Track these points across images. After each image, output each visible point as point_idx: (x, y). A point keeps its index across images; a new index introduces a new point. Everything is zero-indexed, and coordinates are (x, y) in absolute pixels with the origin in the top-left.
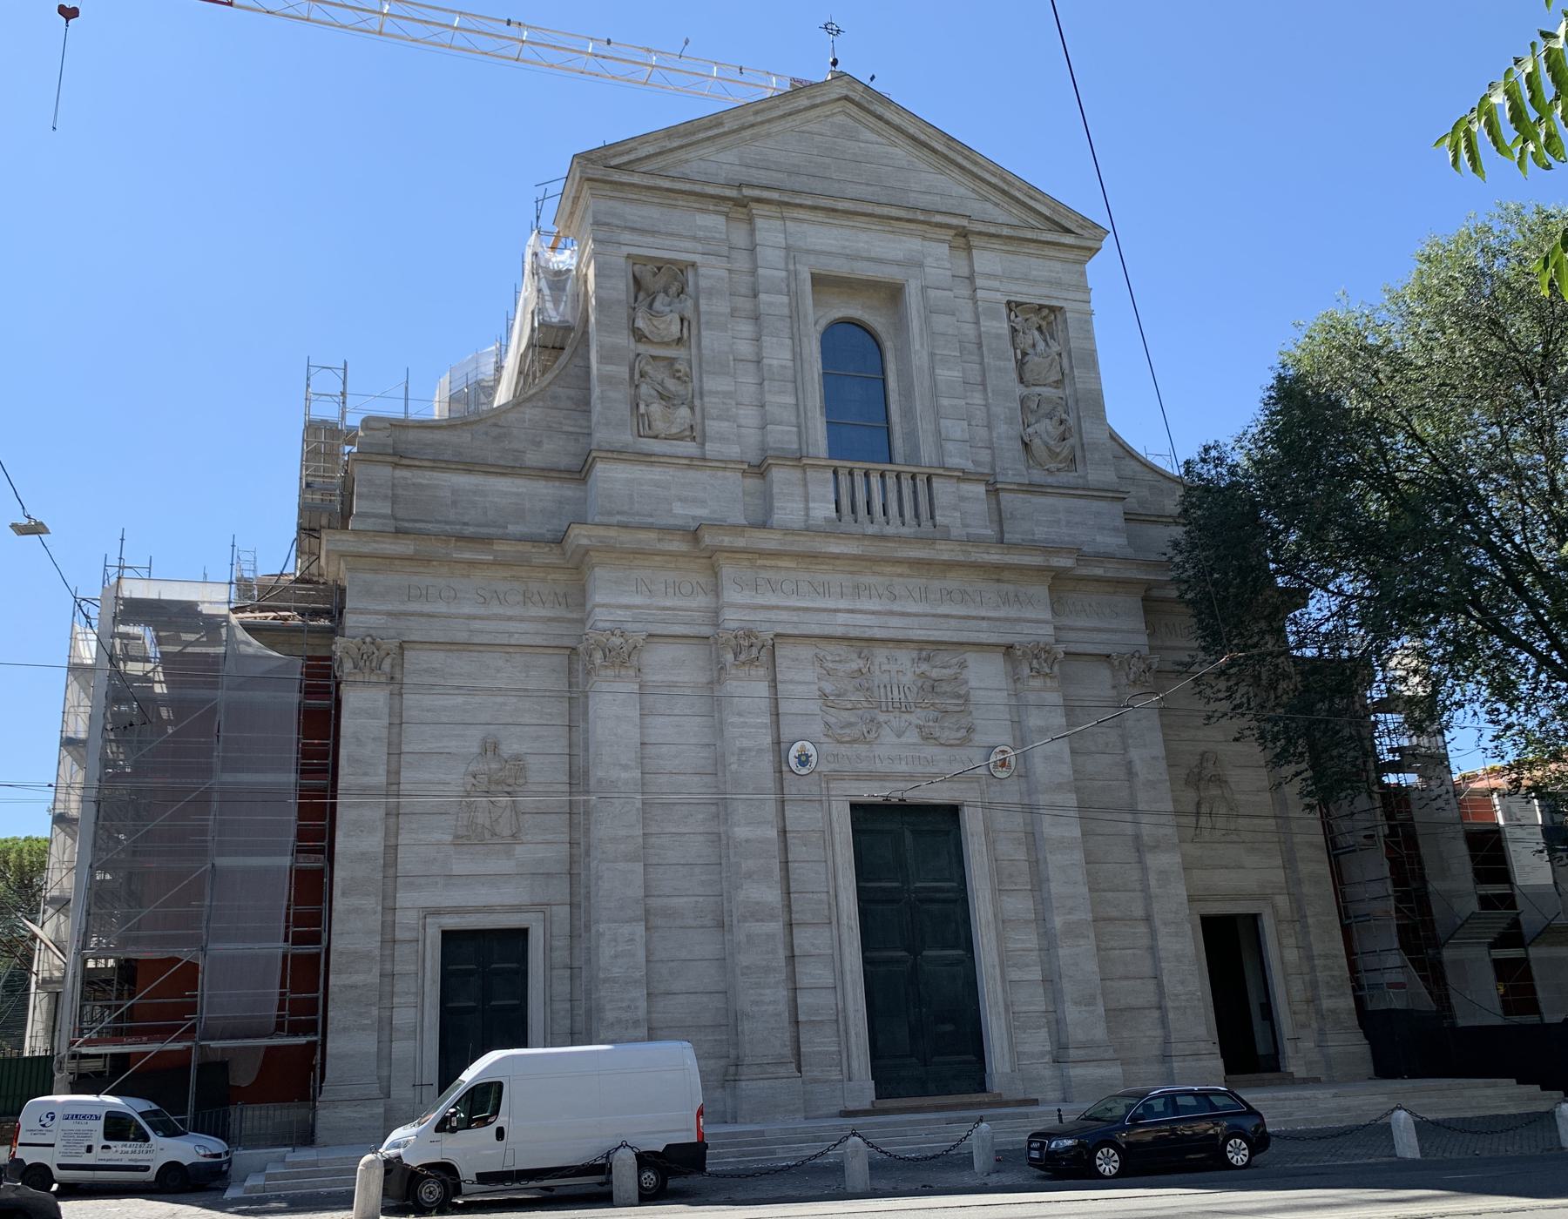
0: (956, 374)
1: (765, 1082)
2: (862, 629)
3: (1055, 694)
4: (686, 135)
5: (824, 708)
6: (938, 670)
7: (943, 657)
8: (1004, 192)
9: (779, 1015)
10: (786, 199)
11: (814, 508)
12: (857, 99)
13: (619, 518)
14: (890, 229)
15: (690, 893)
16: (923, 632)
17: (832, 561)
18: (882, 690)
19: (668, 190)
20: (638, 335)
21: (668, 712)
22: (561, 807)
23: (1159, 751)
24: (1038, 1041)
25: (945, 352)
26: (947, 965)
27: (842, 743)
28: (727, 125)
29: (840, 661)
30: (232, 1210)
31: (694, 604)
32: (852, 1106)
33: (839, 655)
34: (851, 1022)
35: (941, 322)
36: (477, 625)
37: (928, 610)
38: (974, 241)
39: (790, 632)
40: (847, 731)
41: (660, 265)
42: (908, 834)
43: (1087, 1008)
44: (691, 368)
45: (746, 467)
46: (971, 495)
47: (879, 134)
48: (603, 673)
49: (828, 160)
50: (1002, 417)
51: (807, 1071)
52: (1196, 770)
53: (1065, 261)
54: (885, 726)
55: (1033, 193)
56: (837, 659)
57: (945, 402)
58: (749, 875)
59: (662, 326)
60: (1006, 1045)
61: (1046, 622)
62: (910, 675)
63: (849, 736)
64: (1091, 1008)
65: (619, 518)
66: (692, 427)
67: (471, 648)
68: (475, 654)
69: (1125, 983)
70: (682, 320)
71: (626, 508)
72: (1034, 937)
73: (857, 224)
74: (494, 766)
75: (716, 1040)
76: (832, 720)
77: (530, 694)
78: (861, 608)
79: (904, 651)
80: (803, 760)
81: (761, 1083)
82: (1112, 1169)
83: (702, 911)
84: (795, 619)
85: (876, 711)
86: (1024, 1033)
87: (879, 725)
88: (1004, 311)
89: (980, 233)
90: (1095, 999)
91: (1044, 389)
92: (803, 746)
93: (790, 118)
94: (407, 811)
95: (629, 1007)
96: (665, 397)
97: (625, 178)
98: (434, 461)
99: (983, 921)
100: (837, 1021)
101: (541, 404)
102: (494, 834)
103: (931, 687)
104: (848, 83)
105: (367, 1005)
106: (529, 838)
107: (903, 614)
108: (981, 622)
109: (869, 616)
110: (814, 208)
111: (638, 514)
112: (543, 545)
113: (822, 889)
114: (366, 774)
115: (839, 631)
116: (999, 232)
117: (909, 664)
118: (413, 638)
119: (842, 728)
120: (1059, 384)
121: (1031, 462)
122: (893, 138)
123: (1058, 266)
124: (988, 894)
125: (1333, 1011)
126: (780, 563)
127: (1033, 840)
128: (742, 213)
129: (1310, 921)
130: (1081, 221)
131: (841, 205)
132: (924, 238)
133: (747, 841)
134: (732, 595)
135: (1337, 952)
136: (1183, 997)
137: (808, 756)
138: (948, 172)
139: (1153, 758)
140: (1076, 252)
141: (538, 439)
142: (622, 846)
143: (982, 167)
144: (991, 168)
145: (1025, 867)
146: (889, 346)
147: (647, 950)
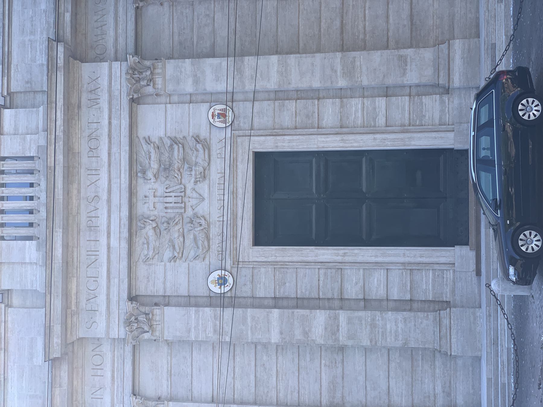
1: (452, 337)
2: (122, 226)
5: (183, 259)
6: (152, 162)
9: (405, 320)
11: (30, 259)
15: (318, 369)
16: (123, 175)
17: (70, 249)
18: (169, 211)
21: (189, 378)
27: (209, 246)
29: (148, 243)
30: (512, 191)
31: (109, 355)
32: (473, 267)
33: (144, 244)
34: (412, 260)
37: (105, 169)
39: (126, 286)
40: (200, 243)
43: (409, 64)
51: (446, 297)
54: (196, 210)
56: (146, 246)
58: (306, 333)
60: (434, 135)
62: (156, 186)
64: (409, 60)
69: (391, 20)
72: (354, 101)
75: (422, 359)
76: (192, 254)
79: (138, 189)
80: (222, 281)
81: (454, 340)
83: (332, 362)
84: (116, 280)
86: (425, 116)
87: (196, 216)
90: (402, 56)
92: (212, 282)
99: (341, 145)
108: (113, 125)
109: (112, 220)
113: (317, 273)
115: (124, 245)
117: (148, 186)
119: (198, 248)
126: (74, 291)
133: (281, 333)
134: (100, 330)
137: (220, 278)
145: (301, 103)
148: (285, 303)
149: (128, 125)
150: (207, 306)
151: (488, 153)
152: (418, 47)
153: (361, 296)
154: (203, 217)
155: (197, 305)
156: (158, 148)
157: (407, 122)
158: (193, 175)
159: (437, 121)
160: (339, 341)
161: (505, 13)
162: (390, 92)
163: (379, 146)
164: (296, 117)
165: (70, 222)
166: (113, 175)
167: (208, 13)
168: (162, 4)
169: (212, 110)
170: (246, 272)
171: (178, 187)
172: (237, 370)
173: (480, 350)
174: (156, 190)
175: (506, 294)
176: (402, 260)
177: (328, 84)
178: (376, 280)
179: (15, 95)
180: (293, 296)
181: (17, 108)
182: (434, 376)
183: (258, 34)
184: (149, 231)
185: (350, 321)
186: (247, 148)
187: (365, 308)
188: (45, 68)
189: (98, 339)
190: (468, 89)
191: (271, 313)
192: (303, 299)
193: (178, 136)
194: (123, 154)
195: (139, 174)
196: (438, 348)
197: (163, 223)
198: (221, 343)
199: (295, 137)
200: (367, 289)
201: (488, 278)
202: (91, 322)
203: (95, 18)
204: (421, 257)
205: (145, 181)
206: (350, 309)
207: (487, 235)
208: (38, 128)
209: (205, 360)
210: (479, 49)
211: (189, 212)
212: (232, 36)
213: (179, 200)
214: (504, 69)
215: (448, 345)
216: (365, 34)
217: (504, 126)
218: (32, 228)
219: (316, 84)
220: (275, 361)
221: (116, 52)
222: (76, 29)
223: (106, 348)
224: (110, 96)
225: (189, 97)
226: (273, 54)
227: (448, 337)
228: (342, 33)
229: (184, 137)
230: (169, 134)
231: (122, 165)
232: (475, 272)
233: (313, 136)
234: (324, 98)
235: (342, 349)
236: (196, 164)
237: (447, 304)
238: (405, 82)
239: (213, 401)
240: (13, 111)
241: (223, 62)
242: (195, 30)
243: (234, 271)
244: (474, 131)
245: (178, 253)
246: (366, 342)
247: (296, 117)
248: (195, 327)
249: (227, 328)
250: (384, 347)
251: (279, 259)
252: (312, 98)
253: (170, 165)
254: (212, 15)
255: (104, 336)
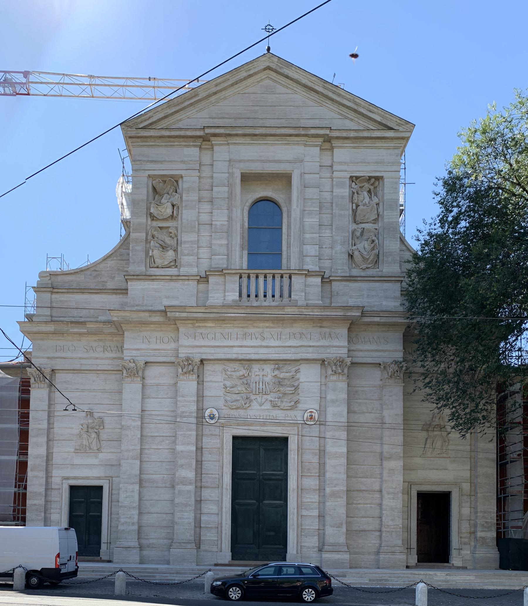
0: (315, 220)
3: (344, 383)
4: (178, 105)
5: (225, 393)
6: (284, 374)
7: (287, 368)
8: (355, 111)
9: (190, 523)
10: (228, 132)
12: (274, 67)
13: (136, 308)
14: (286, 142)
16: (277, 355)
17: (232, 322)
18: (254, 384)
19: (169, 137)
20: (153, 218)
22: (118, 438)
23: (400, 411)
24: (312, 542)
25: (311, 209)
26: (276, 507)
27: (233, 409)
28: (200, 95)
29: (235, 371)
30: (262, 584)
32: (220, 562)
33: (235, 368)
34: (223, 529)
35: (311, 193)
36: (84, 362)
38: (335, 143)
40: (235, 403)
41: (164, 179)
42: (262, 451)
43: (337, 529)
44: (177, 231)
45: (198, 278)
46: (313, 283)
47: (287, 88)
48: (126, 380)
49: (256, 108)
50: (339, 242)
52: (428, 423)
53: (388, 148)
54: (254, 401)
55: (371, 108)
56: (233, 370)
57: (307, 236)
58: (182, 466)
59: (163, 211)
60: (295, 542)
61: (343, 347)
62: (270, 376)
63: (235, 405)
64: (339, 529)
65: (136, 308)
66: (175, 260)
67: (83, 372)
68: (85, 374)
69: (363, 519)
70: (173, 206)
71: (140, 303)
72: (317, 497)
73: (269, 142)
74: (90, 421)
75: (168, 532)
76: (229, 399)
77: (106, 391)
78: (246, 345)
80: (212, 417)
81: (178, 550)
82: (236, 597)
83: (165, 481)
84: (213, 352)
85: (251, 394)
87: (251, 401)
88: (347, 181)
89: (338, 138)
91: (367, 225)
92: (212, 411)
93: (236, 86)
94: (57, 439)
95: (130, 517)
96: (164, 248)
97: (152, 133)
98: (67, 289)
99: (291, 489)
100: (218, 528)
101: (115, 258)
102: (90, 449)
103: (280, 382)
104: (269, 58)
105: (40, 512)
106: (104, 450)
107: (267, 347)
110: (245, 135)
111: (146, 305)
112: (107, 324)
114: (39, 424)
115: (234, 356)
116: (349, 135)
117: (269, 371)
118: (57, 368)
119: (232, 402)
120: (376, 221)
121: (354, 265)
122: (295, 89)
123: (383, 152)
124: (295, 478)
125: (483, 538)
127: (322, 453)
128: (209, 145)
129: (479, 495)
130: (398, 121)
131: (257, 132)
132: (306, 145)
133: (182, 452)
134: (184, 341)
135: (492, 510)
136: (392, 527)
138: (324, 104)
139: (396, 415)
140: (396, 141)
141: (113, 276)
142: (131, 453)
143: (343, 97)
144: (348, 96)
146: (284, 209)
147: (139, 496)
148: (199, 454)
149: (309, 358)
150: (197, 407)
151: (285, 572)
152: (347, 534)
153: (203, 498)
154: (250, 406)
155: (198, 401)
156: (293, 378)
157: (303, 527)
158: (275, 400)
159: (303, 544)
160: (178, 485)
161: (363, 583)
162: (321, 518)
163: (290, 511)
164: (309, 462)
165: (249, 322)
166: (277, 349)
167: (375, 409)
168: (381, 380)
169: (315, 411)
170: (217, 431)
171: (268, 390)
172: (161, 425)
173: (173, 565)
174: (267, 376)
175: (205, 580)
176: (224, 522)
177: (328, 482)
178: (212, 507)
179: (330, 285)
180: (203, 459)
181: (322, 286)
182: (159, 538)
183: (360, 440)
184: (242, 372)
185: (189, 492)
186: (291, 433)
187: (196, 501)
188: (346, 305)
189: (178, 340)
190: (321, 562)
191: (194, 446)
192: (201, 465)
193: (299, 390)
194: (290, 355)
195: (277, 366)
196: (174, 541)
197: (247, 381)
198: (176, 417)
199: (296, 462)
200: (207, 502)
201: (214, 570)
202: (188, 336)
203: (375, 337)
204: (225, 534)
205: (273, 370)
206: (196, 492)
207: (238, 570)
208: (309, 300)
209: (166, 406)
210: (343, 568)
211: (253, 397)
212: (359, 424)
213: (261, 391)
214: (332, 581)
215: (176, 547)
216: (356, 504)
217: (300, 581)
218: (246, 296)
219: (328, 475)
220: (166, 447)
221: (353, 350)
222: (369, 325)
223: (173, 345)
224: (327, 347)
225: (324, 396)
226: (347, 449)
227: (180, 547)
228: (358, 491)
229: (299, 394)
230: (301, 384)
231: (283, 355)
232: (216, 563)
233: (297, 472)
234: (319, 479)
235: (173, 487)
236: (282, 401)
237: (198, 547)
238: (327, 527)
239: (142, 411)
240: (320, 284)
241: (344, 419)
242: (365, 401)
243: (218, 424)
244: (298, 565)
245: (229, 390)
246: (177, 501)
247: (309, 462)
248: (185, 400)
249: (184, 420)
250: (174, 511)
251: (225, 450)
252: (319, 472)
253: (282, 385)
254: (373, 412)
255: (180, 344)
